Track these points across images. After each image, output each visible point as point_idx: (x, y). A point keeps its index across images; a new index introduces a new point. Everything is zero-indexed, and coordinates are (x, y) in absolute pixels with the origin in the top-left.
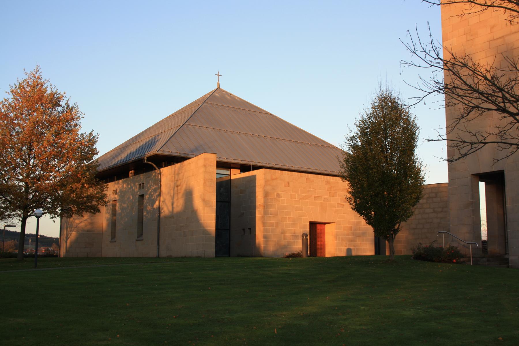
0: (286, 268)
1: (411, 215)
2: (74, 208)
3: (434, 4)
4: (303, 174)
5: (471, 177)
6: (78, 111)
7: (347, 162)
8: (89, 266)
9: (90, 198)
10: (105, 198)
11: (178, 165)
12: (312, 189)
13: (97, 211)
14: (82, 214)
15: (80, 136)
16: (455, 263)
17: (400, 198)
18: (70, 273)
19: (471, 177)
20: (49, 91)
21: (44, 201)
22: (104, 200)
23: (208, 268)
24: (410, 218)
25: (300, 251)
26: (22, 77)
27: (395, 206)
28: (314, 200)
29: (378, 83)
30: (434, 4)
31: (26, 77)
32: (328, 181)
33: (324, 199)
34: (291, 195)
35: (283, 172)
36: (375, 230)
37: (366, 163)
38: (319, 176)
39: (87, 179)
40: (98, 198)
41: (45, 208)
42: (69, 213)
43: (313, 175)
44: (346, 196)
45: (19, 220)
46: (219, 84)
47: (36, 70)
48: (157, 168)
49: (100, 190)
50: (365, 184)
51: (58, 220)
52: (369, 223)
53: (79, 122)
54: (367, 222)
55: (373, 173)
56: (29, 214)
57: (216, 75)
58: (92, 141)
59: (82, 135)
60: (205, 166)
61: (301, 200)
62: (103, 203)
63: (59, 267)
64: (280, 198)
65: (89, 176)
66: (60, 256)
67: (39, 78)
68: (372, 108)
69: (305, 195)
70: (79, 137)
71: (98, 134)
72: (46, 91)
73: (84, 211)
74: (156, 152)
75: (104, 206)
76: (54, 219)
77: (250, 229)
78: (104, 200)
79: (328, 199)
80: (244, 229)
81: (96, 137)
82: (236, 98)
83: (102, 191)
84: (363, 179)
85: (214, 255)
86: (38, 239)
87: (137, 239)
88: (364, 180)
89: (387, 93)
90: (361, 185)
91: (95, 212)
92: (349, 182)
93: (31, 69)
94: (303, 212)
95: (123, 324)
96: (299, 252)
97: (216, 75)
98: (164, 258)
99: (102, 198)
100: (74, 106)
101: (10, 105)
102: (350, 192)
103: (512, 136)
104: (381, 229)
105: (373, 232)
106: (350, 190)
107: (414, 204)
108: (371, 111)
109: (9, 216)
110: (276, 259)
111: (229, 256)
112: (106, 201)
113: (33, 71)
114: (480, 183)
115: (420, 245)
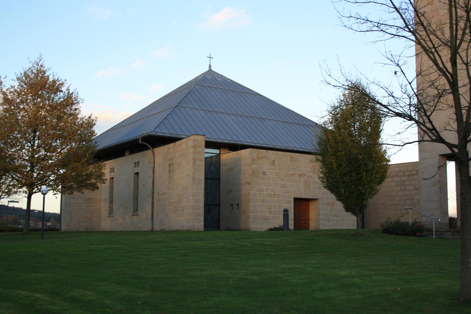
1: (376, 193)
2: (74, 185)
3: (357, 31)
4: (288, 153)
5: (438, 157)
6: (78, 97)
7: (320, 144)
8: (89, 238)
9: (89, 176)
10: (103, 177)
11: (171, 145)
12: (296, 167)
13: (95, 188)
14: (82, 191)
15: (80, 119)
16: (418, 236)
17: (366, 177)
18: (73, 243)
19: (438, 157)
20: (51, 79)
21: (48, 179)
22: (102, 178)
23: (193, 239)
25: (282, 225)
26: (27, 66)
27: (361, 185)
28: (299, 177)
30: (357, 31)
31: (30, 65)
33: (308, 176)
34: (276, 172)
35: (269, 151)
38: (303, 155)
39: (86, 159)
40: (96, 177)
41: (50, 186)
42: (69, 190)
43: (297, 154)
44: (319, 175)
45: (25, 196)
46: (210, 66)
47: (40, 58)
48: (151, 148)
49: (99, 169)
50: (334, 165)
51: (59, 195)
52: (339, 200)
53: (79, 106)
54: (337, 199)
55: (341, 155)
56: (34, 191)
57: (208, 57)
58: (90, 124)
59: (82, 119)
60: (194, 147)
61: (285, 178)
62: (101, 181)
63: (63, 238)
65: (88, 156)
66: (60, 230)
67: (41, 66)
69: (290, 172)
70: (79, 120)
71: (96, 117)
72: (49, 79)
73: (84, 188)
74: (150, 133)
75: (102, 184)
76: (56, 195)
77: (238, 205)
78: (102, 178)
79: (311, 177)
80: (232, 205)
81: (95, 120)
82: (226, 79)
83: (100, 169)
84: (333, 161)
85: (203, 229)
86: (43, 215)
87: (132, 214)
88: (333, 162)
90: (331, 166)
91: (94, 189)
92: (321, 163)
93: (34, 58)
94: (288, 188)
95: (118, 277)
96: (281, 226)
97: (208, 57)
98: (158, 231)
99: (100, 176)
100: (75, 92)
101: (16, 91)
102: (321, 172)
103: (397, 139)
104: (349, 205)
106: (321, 170)
107: (380, 182)
109: (16, 193)
111: (219, 230)
112: (104, 179)
113: (36, 59)
115: (388, 220)
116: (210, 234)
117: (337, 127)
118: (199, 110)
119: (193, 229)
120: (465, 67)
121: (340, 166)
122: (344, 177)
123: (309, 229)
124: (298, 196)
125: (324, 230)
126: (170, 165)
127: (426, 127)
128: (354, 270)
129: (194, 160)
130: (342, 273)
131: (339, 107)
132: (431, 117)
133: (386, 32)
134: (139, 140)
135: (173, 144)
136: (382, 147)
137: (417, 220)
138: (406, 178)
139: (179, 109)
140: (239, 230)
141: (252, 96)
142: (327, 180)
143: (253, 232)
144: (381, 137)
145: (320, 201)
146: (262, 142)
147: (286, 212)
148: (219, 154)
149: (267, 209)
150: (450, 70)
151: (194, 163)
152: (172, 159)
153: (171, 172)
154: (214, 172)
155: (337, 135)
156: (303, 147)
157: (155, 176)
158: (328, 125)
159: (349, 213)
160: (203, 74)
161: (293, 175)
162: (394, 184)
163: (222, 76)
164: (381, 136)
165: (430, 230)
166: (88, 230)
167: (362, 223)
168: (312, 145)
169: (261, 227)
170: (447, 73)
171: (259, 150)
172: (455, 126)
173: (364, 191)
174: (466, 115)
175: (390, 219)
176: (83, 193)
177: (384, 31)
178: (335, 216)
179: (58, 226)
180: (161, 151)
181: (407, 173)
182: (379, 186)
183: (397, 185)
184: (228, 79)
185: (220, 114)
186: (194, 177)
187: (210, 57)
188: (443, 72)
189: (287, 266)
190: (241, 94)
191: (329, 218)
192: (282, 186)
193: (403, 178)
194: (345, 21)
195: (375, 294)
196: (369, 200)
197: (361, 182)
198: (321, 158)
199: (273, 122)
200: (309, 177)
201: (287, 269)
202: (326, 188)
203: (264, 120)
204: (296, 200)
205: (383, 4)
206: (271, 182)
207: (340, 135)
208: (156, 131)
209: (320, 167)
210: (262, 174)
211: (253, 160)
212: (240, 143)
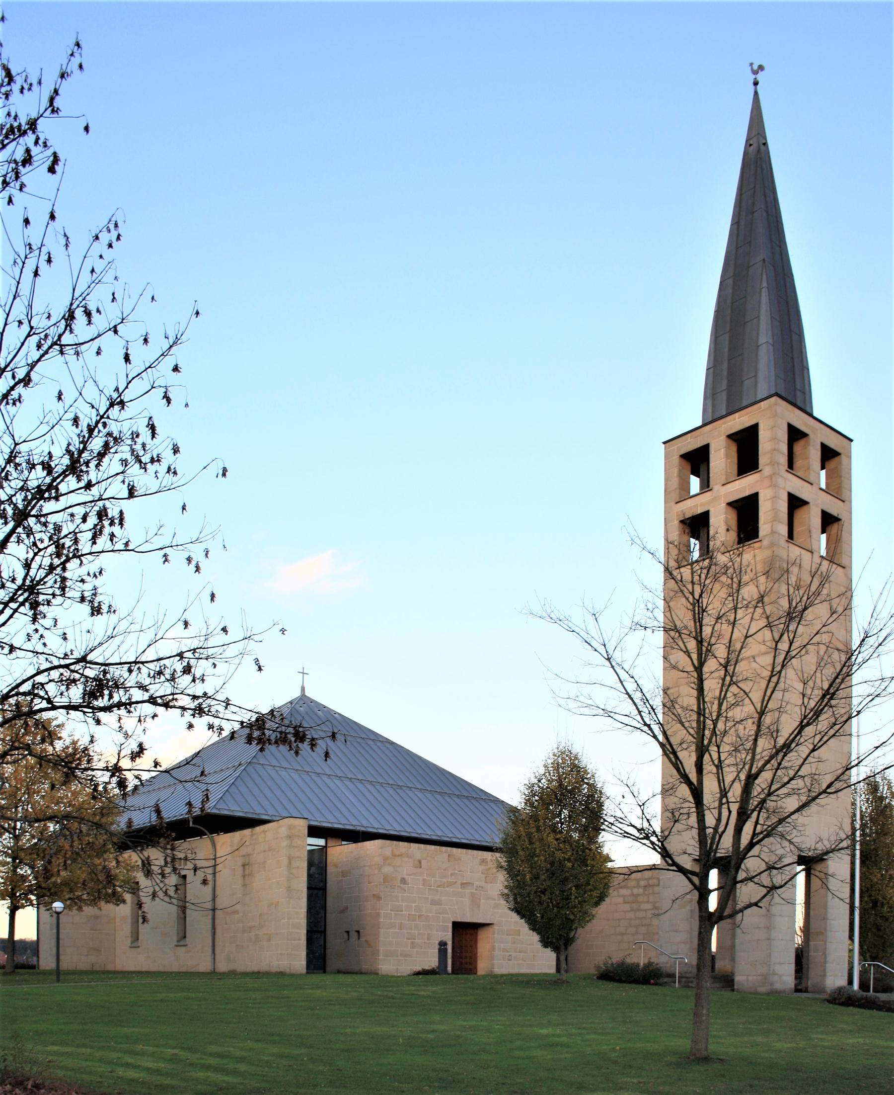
0: (413, 988)
4: (444, 848)
11: (247, 832)
16: (653, 984)
24: (589, 924)
34: (424, 880)
36: (541, 938)
38: (470, 851)
46: (303, 689)
52: (533, 930)
60: (290, 837)
77: (358, 932)
82: (333, 713)
85: (305, 971)
87: (176, 943)
98: (224, 974)
104: (548, 938)
106: (506, 883)
107: (597, 904)
108: (542, 771)
110: (399, 977)
111: (325, 972)
115: (608, 959)
116: (318, 978)
118: (288, 770)
119: (288, 971)
121: (536, 877)
122: (542, 895)
123: (476, 973)
125: (502, 976)
126: (244, 865)
129: (290, 859)
130: (544, 1031)
134: (189, 821)
135: (249, 830)
137: (652, 961)
138: (641, 891)
139: (254, 768)
140: (360, 973)
141: (379, 744)
142: (515, 899)
143: (383, 976)
145: (496, 927)
146: (398, 828)
147: (443, 944)
148: (326, 847)
149: (408, 939)
151: (290, 863)
152: (249, 855)
153: (247, 877)
154: (317, 876)
156: (470, 837)
157: (218, 883)
159: (549, 950)
160: (291, 702)
161: (451, 884)
162: (621, 900)
163: (325, 707)
165: (672, 976)
166: (94, 969)
173: (572, 917)
175: (610, 958)
176: (100, 909)
178: (520, 952)
179: (34, 961)
180: (226, 841)
183: (625, 903)
185: (325, 778)
186: (289, 887)
187: (303, 673)
189: (465, 1023)
192: (434, 903)
193: (636, 891)
196: (580, 930)
197: (569, 903)
200: (480, 888)
202: (512, 910)
208: (218, 806)
209: (504, 879)
211: (386, 859)
212: (363, 829)
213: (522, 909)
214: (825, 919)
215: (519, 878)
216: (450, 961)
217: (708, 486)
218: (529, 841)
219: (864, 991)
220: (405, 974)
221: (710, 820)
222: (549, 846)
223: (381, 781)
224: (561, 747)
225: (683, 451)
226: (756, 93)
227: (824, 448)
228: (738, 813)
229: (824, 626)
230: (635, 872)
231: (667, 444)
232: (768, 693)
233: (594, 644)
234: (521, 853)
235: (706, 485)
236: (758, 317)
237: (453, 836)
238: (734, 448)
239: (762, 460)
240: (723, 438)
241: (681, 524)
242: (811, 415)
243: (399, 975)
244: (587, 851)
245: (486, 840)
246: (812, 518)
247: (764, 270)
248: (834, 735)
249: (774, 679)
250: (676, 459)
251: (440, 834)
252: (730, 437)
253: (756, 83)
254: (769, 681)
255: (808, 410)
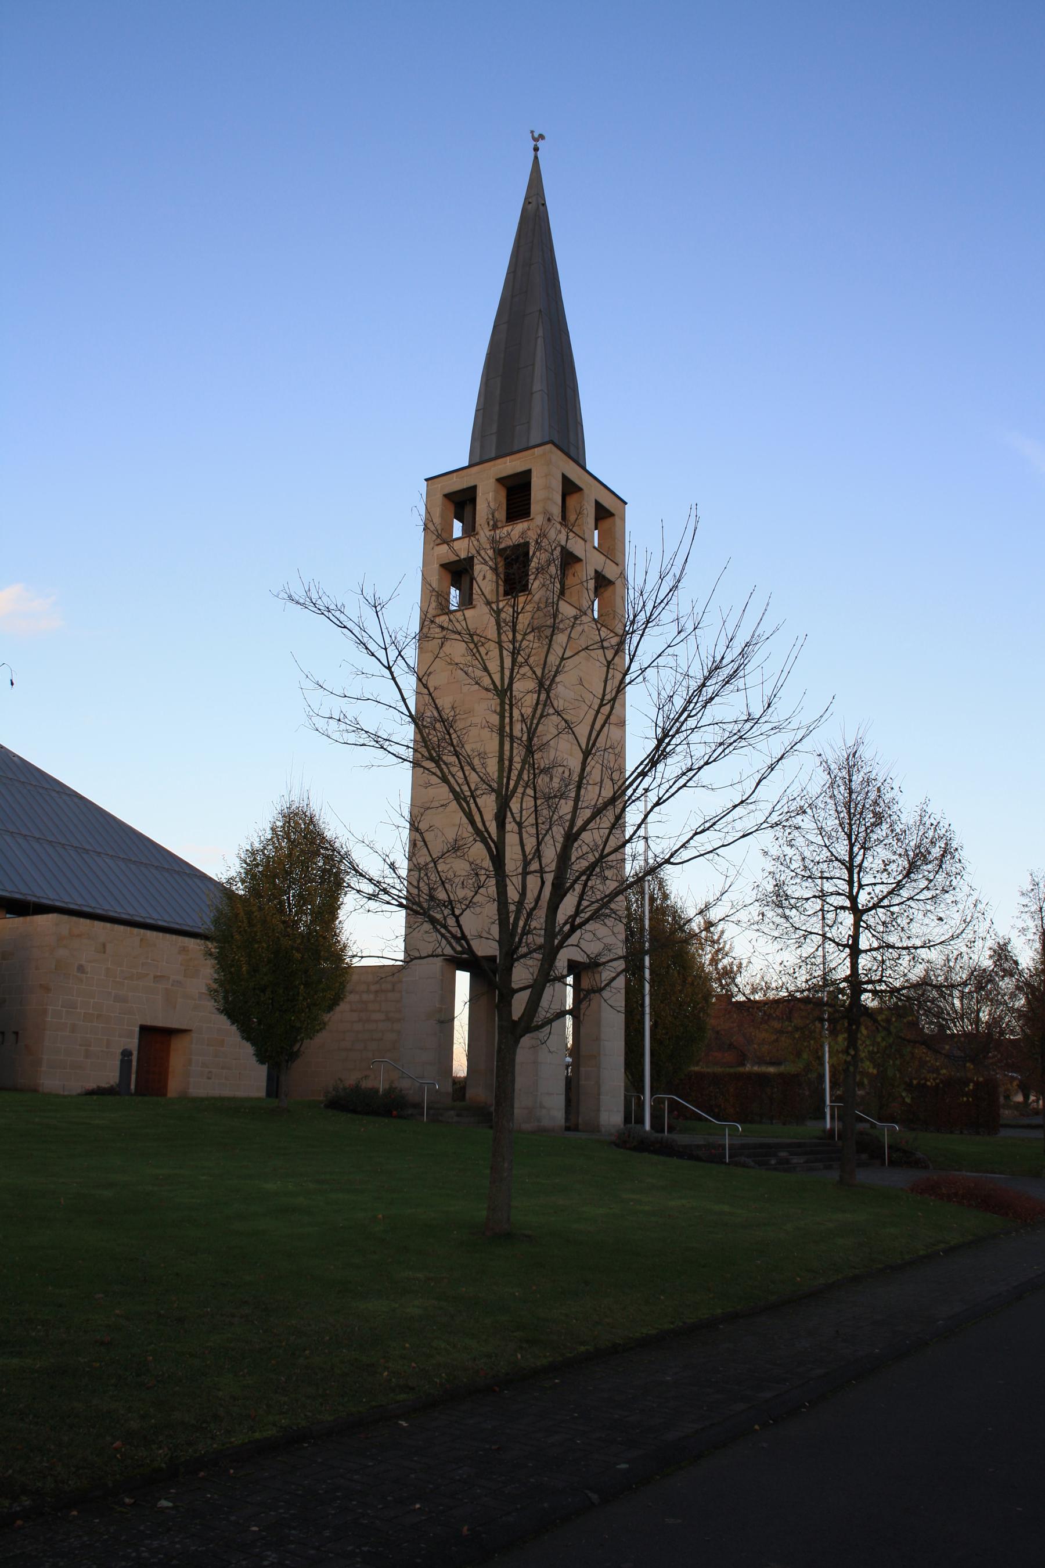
1: (321, 1029)
4: (136, 930)
7: (216, 923)
16: (395, 1117)
24: (319, 1035)
29: (287, 786)
32: (184, 947)
35: (96, 923)
36: (256, 1050)
37: (249, 930)
38: (168, 936)
43: (155, 933)
54: (243, 1037)
64: (85, 975)
68: (272, 829)
77: (16, 1033)
84: (242, 959)
89: (301, 805)
96: (112, 1086)
102: (216, 979)
105: (254, 1054)
106: (216, 976)
107: (330, 1008)
110: (65, 1096)
114: (458, 973)
115: (339, 1082)
117: (254, 891)
120: (516, 828)
122: (262, 994)
123: (164, 1094)
124: (149, 1022)
125: (202, 1099)
127: (449, 932)
128: (290, 1182)
131: (262, 851)
132: (461, 919)
133: (389, 752)
136: (339, 938)
138: (372, 997)
142: (225, 998)
144: (339, 919)
146: (80, 901)
147: (126, 1054)
149: (80, 1045)
150: (494, 836)
155: (255, 909)
156: (168, 919)
158: (236, 885)
164: (340, 916)
165: (418, 1106)
167: (274, 1087)
168: (203, 921)
169: (64, 1085)
170: (489, 840)
171: (74, 919)
172: (495, 930)
173: (298, 1025)
174: (513, 916)
175: (341, 1080)
177: (385, 749)
181: (373, 988)
182: (329, 1015)
183: (352, 1011)
184: (15, 755)
188: (481, 835)
190: (41, 791)
191: (210, 1072)
193: (365, 997)
194: (321, 723)
195: (341, 1225)
196: (306, 1042)
198: (218, 953)
199: (107, 860)
201: (161, 1177)
202: (222, 1012)
203: (88, 853)
204: (144, 1030)
205: (390, 706)
206: (95, 988)
207: (260, 909)
210: (76, 970)
212: (34, 899)
213: (233, 1011)
214: (598, 1039)
215: (233, 969)
216: (134, 1077)
217: (474, 531)
218: (249, 922)
219: (657, 1132)
220: (74, 1093)
221: (513, 895)
222: (273, 930)
223: (63, 842)
224: (294, 807)
225: (446, 491)
226: (536, 158)
227: (598, 506)
228: (553, 884)
229: (669, 646)
230: (416, 958)
231: (430, 482)
232: (597, 727)
233: (372, 647)
234: (237, 937)
235: (470, 530)
236: (533, 365)
237: (148, 915)
238: (503, 493)
239: (535, 508)
240: (492, 481)
241: (441, 569)
242: (584, 468)
243: (66, 1093)
244: (320, 939)
245: (189, 924)
246: (586, 572)
247: (540, 321)
248: (685, 785)
249: (606, 709)
250: (439, 498)
251: (132, 912)
252: (500, 480)
253: (536, 149)
254: (598, 712)
255: (581, 462)
